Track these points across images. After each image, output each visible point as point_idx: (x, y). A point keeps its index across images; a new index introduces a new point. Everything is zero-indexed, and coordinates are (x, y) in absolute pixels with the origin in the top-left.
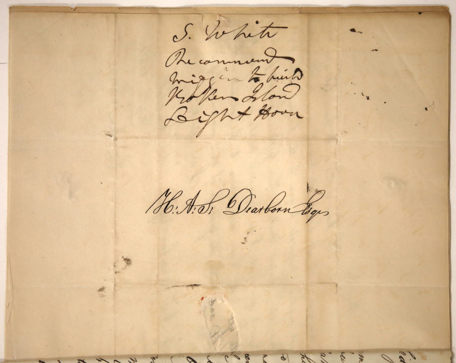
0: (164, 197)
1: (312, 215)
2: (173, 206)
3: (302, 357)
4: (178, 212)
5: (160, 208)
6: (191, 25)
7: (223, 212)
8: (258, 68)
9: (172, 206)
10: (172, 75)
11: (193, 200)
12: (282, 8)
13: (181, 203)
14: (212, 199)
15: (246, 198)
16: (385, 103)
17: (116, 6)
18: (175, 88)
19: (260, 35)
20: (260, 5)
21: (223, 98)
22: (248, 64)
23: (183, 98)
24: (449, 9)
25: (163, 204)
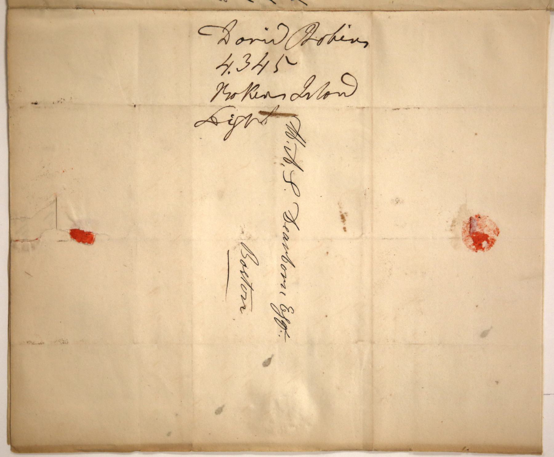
5: (277, 313)
7: (285, 147)
8: (226, 138)
9: (201, 31)
11: (246, 118)
12: (213, 451)
17: (414, 452)
20: (241, 454)
23: (230, 93)
24: (11, 449)
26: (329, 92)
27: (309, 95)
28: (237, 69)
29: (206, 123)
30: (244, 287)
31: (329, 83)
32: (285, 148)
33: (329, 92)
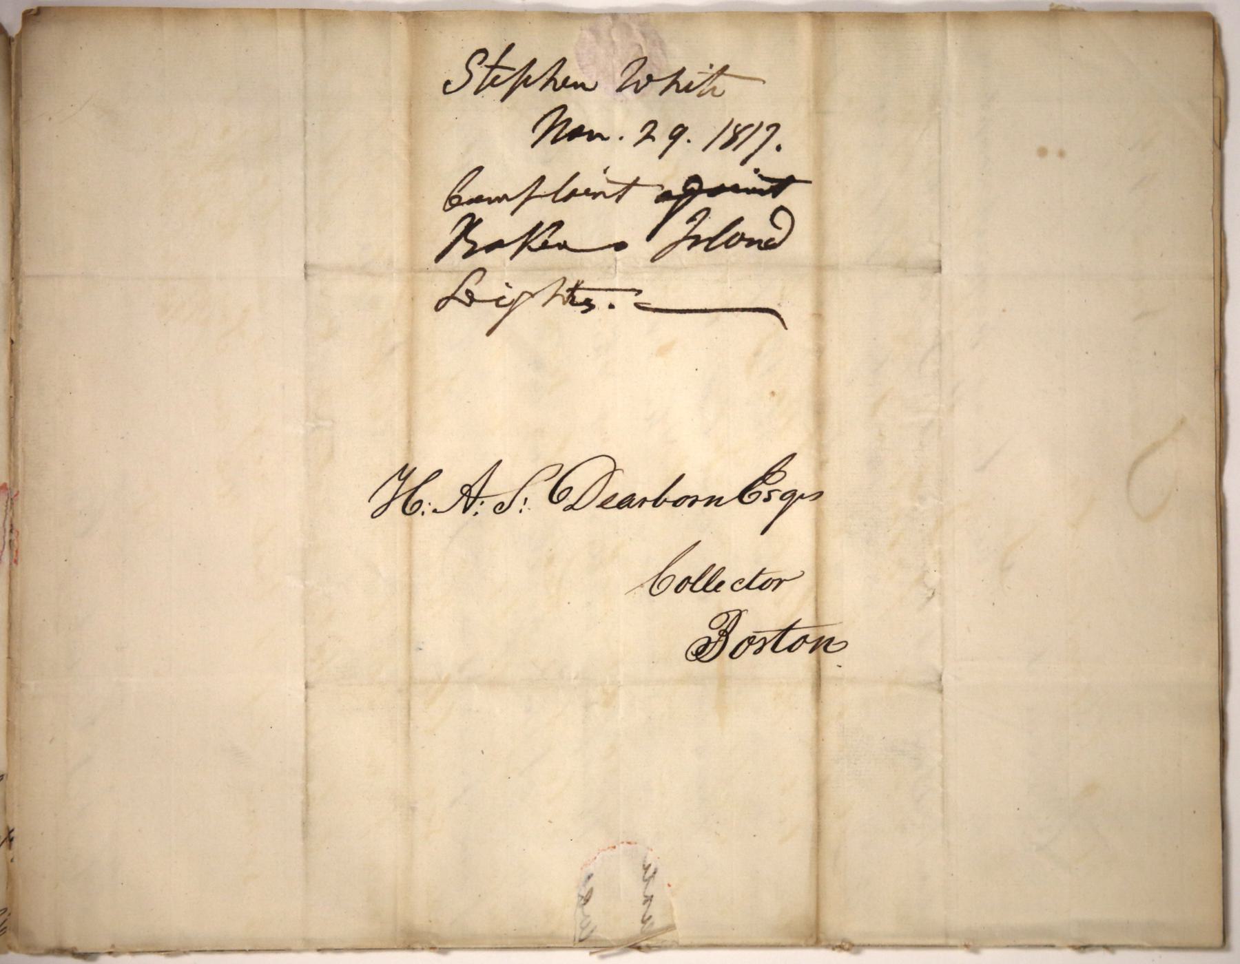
0: (395, 483)
1: (402, 482)
2: (675, 576)
3: (716, 505)
6: (762, 172)
9: (673, 577)
13: (439, 494)
14: (678, 484)
15: (588, 460)
19: (397, 476)
22: (742, 505)
25: (393, 499)
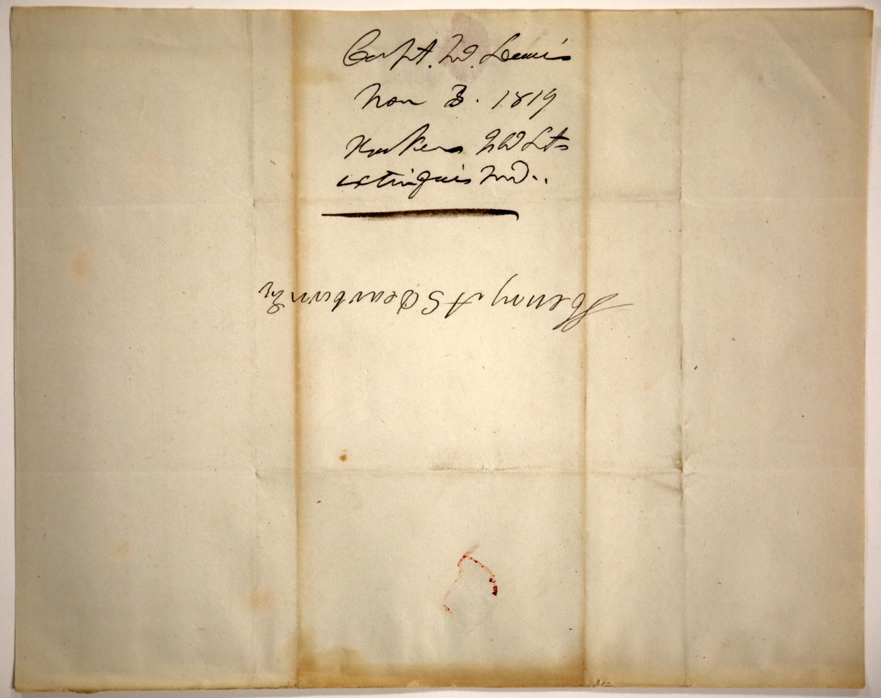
4: (480, 298)
10: (513, 277)
16: (478, 101)
18: (518, 304)
21: (403, 102)
26: (396, 98)
27: (303, 299)
28: (518, 93)
29: (492, 57)
30: (351, 51)
31: (492, 305)
32: (411, 40)
33: (396, 98)
